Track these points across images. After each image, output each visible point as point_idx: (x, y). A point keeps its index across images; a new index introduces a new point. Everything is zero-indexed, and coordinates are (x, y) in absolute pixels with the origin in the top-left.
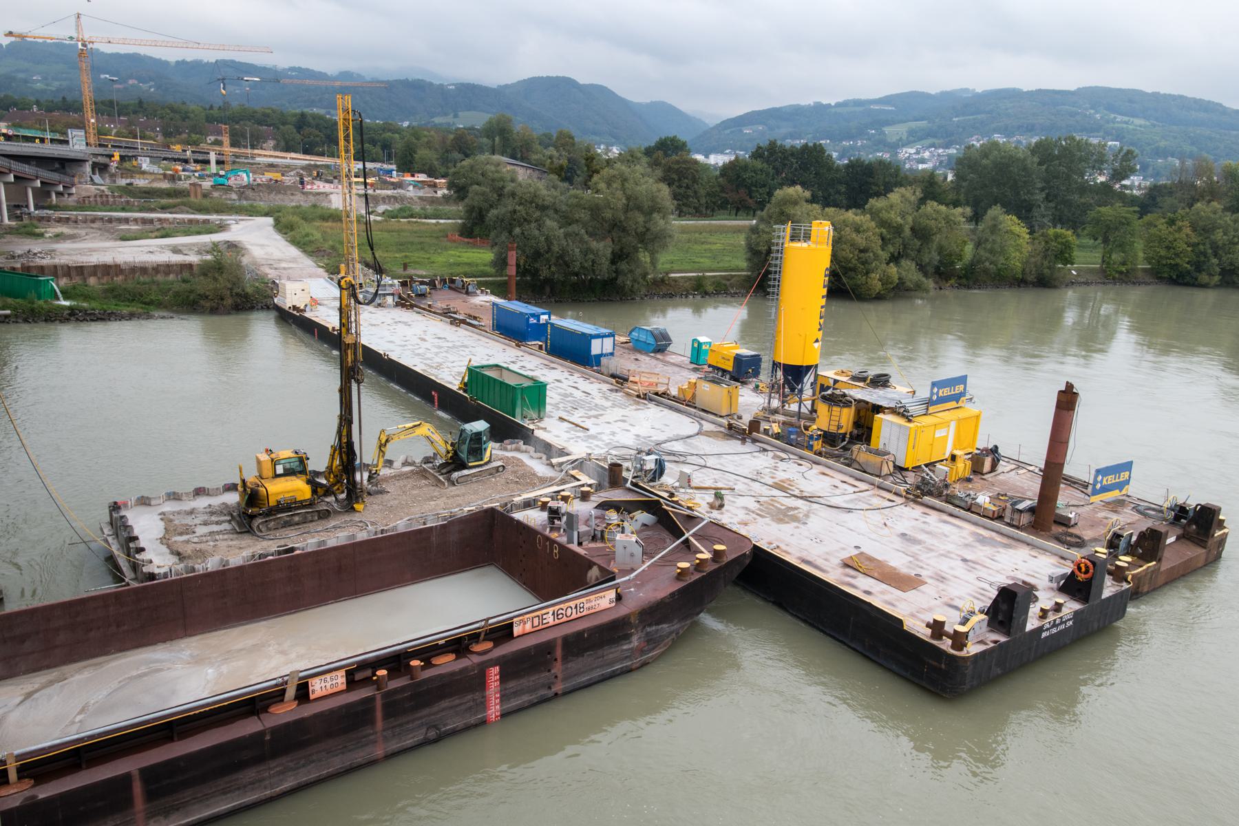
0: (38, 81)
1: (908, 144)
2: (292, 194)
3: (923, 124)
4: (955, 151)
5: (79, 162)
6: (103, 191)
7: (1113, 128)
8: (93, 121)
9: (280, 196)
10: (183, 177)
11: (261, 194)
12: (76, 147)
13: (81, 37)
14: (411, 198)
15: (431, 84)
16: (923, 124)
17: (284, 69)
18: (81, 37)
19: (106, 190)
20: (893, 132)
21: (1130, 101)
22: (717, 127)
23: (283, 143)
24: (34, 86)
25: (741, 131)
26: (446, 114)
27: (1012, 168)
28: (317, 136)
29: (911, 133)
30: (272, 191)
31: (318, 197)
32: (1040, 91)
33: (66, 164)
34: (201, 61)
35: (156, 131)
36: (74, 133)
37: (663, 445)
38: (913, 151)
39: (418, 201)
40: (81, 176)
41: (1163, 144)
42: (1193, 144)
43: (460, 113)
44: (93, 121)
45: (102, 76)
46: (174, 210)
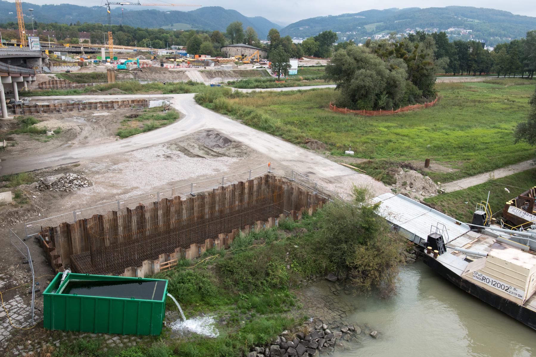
1: (377, 32)
2: (164, 73)
3: (382, 24)
4: (400, 36)
5: (35, 59)
6: (53, 78)
7: (468, 24)
8: (24, 32)
9: (158, 75)
10: (87, 64)
11: (147, 74)
12: (34, 49)
14: (229, 72)
15: (159, 11)
16: (382, 24)
17: (91, 7)
19: (55, 77)
20: (369, 28)
21: (471, 12)
22: (288, 27)
23: (117, 41)
25: (299, 29)
26: (167, 25)
27: (284, 42)
28: (129, 36)
29: (377, 28)
30: (152, 72)
31: (179, 74)
32: (432, 8)
33: (27, 60)
34: (53, 5)
35: (53, 37)
36: (32, 40)
37: (451, 243)
38: (381, 36)
39: (233, 73)
40: (37, 68)
41: (492, 30)
42: (504, 30)
43: (174, 24)
44: (24, 32)
45: (10, 13)
46: (111, 91)
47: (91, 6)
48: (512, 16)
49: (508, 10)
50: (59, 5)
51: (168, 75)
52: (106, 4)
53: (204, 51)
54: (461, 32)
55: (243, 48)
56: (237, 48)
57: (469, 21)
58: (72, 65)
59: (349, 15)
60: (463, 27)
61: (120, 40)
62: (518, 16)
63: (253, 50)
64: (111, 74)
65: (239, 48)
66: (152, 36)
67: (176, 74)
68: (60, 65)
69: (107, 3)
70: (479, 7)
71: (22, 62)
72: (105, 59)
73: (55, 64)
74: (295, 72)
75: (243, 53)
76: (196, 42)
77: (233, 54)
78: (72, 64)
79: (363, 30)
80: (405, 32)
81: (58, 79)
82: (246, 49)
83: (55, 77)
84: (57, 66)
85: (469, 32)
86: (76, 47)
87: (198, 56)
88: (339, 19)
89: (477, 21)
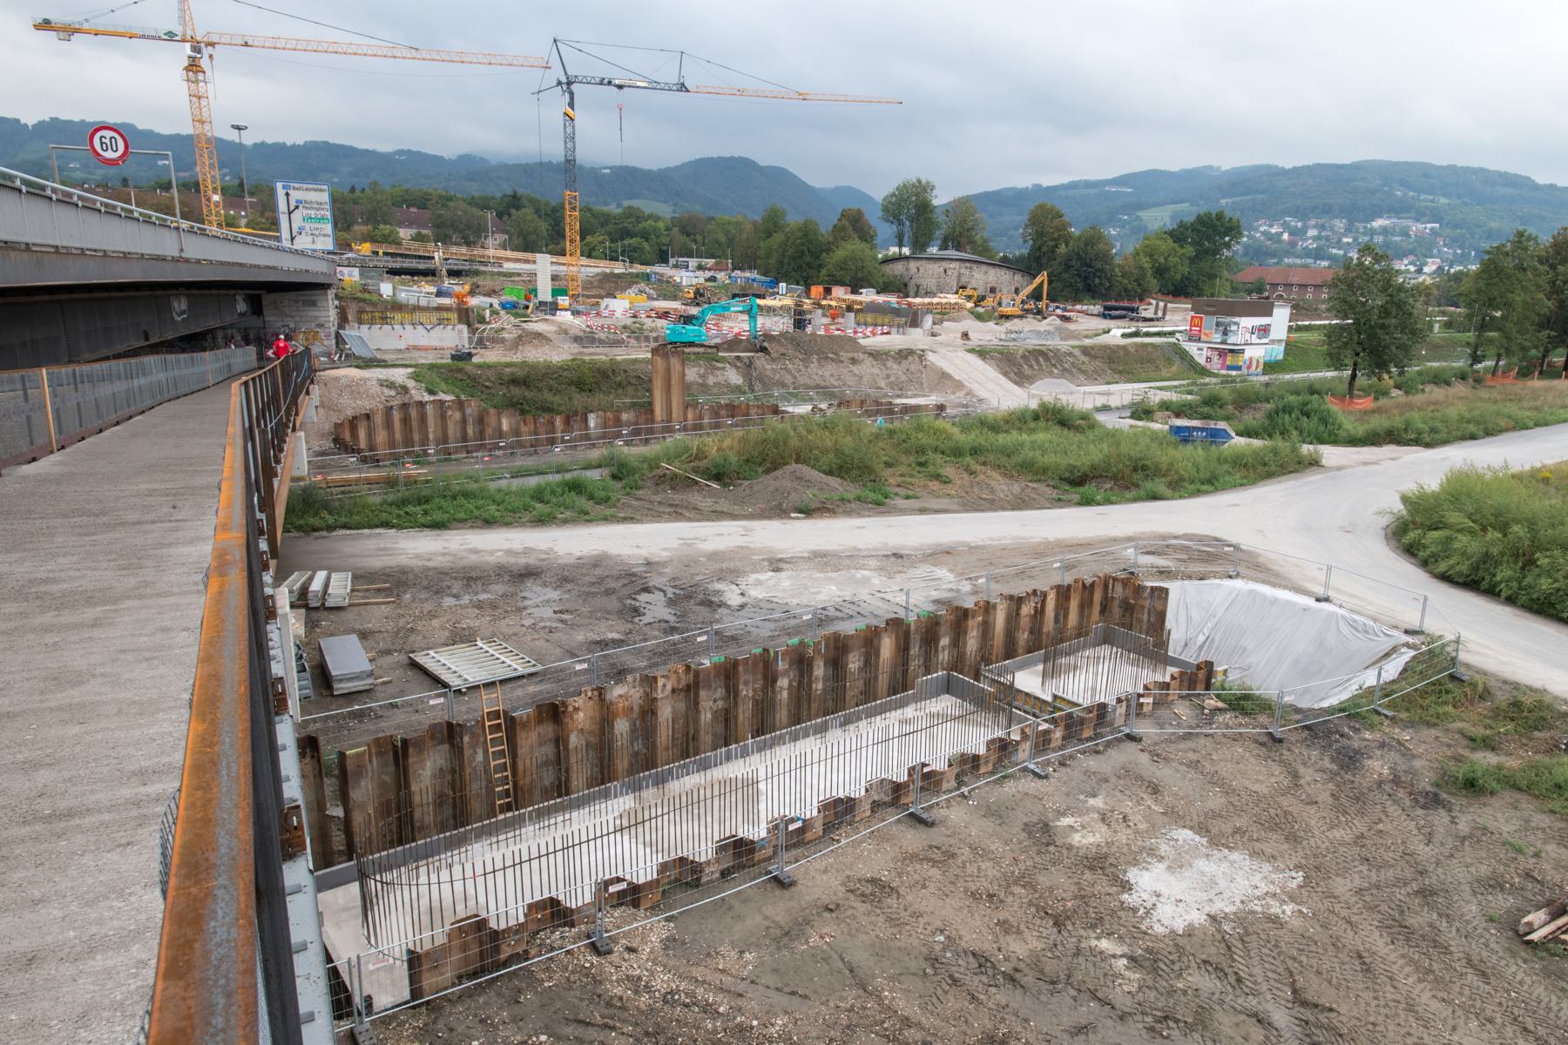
0: (77, 169)
5: (304, 290)
6: (405, 389)
12: (303, 243)
13: (189, 33)
14: (1070, 354)
18: (189, 33)
19: (411, 384)
24: (71, 174)
32: (1318, 166)
33: (267, 299)
36: (295, 195)
41: (1494, 225)
47: (391, 150)
48: (1536, 187)
49: (1523, 171)
50: (302, 143)
51: (868, 368)
52: (559, 83)
53: (838, 274)
54: (1409, 228)
55: (963, 265)
56: (945, 264)
57: (1424, 201)
58: (434, 320)
59: (1089, 184)
60: (1413, 215)
61: (525, 238)
62: (1552, 187)
63: (998, 270)
64: (668, 370)
65: (953, 265)
66: (611, 227)
67: (895, 366)
68: (385, 320)
69: (564, 80)
70: (1445, 163)
71: (241, 306)
72: (549, 299)
73: (365, 317)
74: (237, 297)
75: (963, 280)
76: (810, 242)
77: (930, 283)
78: (434, 317)
79: (1135, 224)
80: (1256, 229)
81: (427, 397)
82: (975, 266)
83: (411, 384)
84: (372, 323)
85: (1432, 229)
86: (392, 255)
87: (820, 289)
88: (1064, 193)
89: (1443, 201)
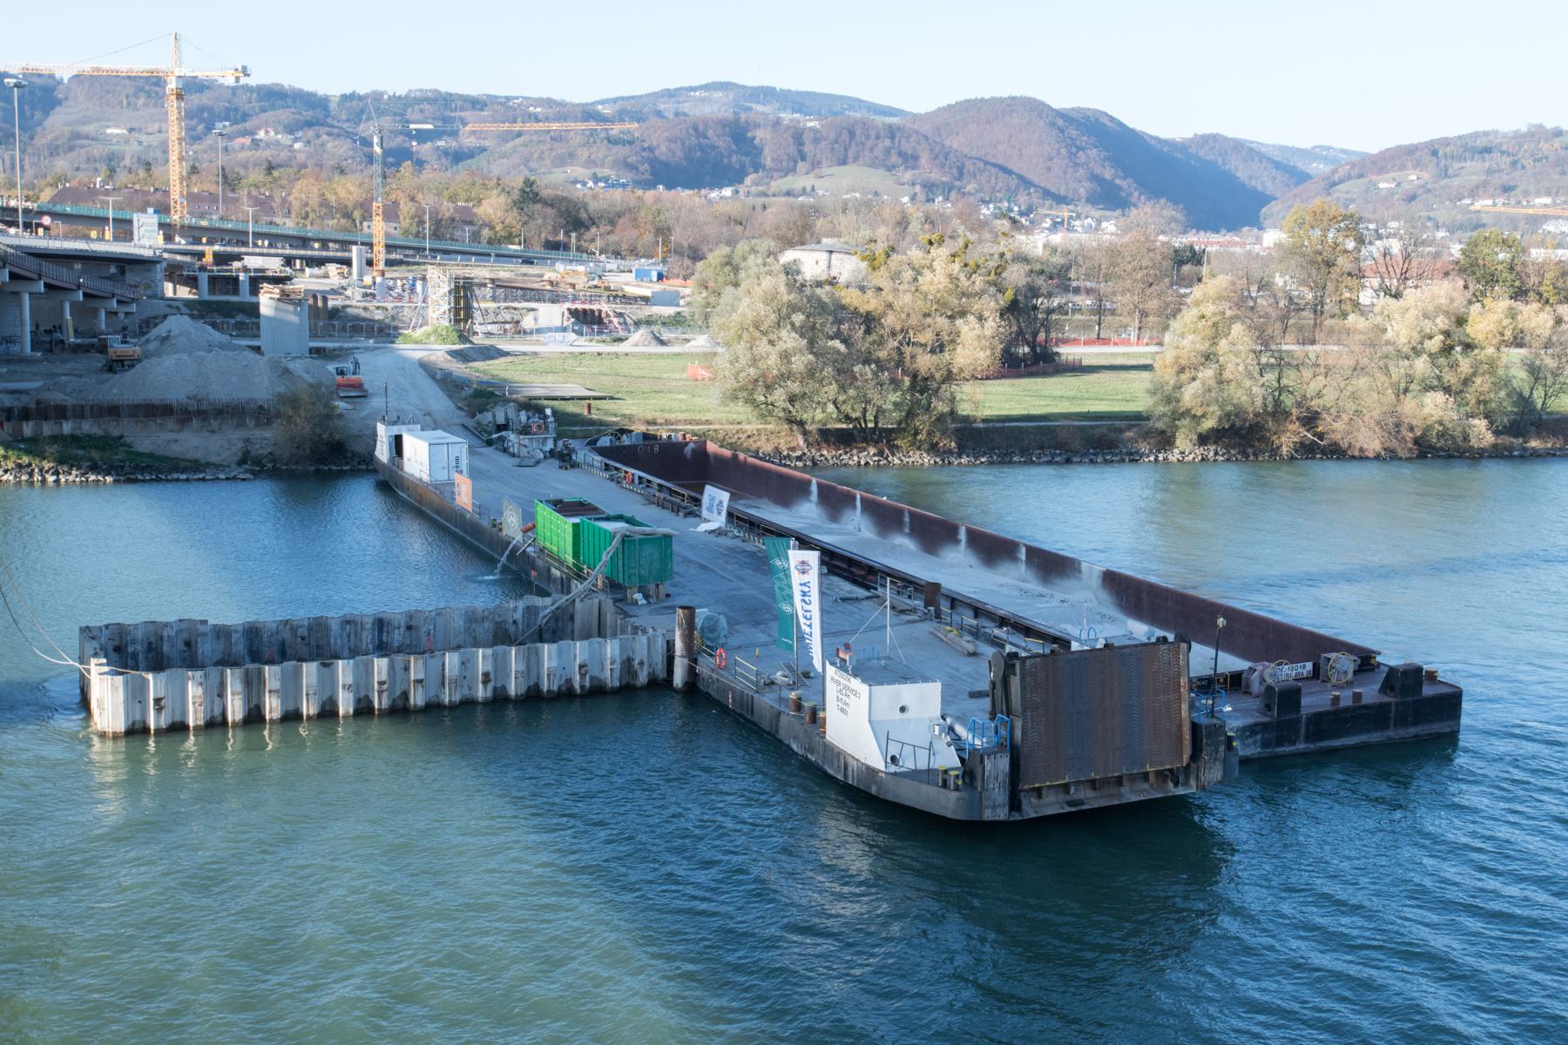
33: (128, 268)
36: (142, 220)
71: (113, 270)
